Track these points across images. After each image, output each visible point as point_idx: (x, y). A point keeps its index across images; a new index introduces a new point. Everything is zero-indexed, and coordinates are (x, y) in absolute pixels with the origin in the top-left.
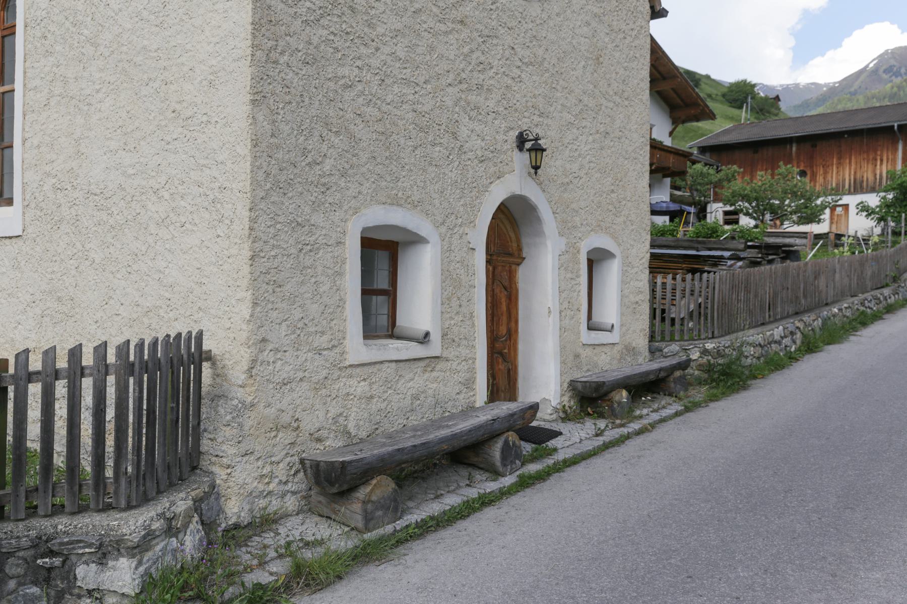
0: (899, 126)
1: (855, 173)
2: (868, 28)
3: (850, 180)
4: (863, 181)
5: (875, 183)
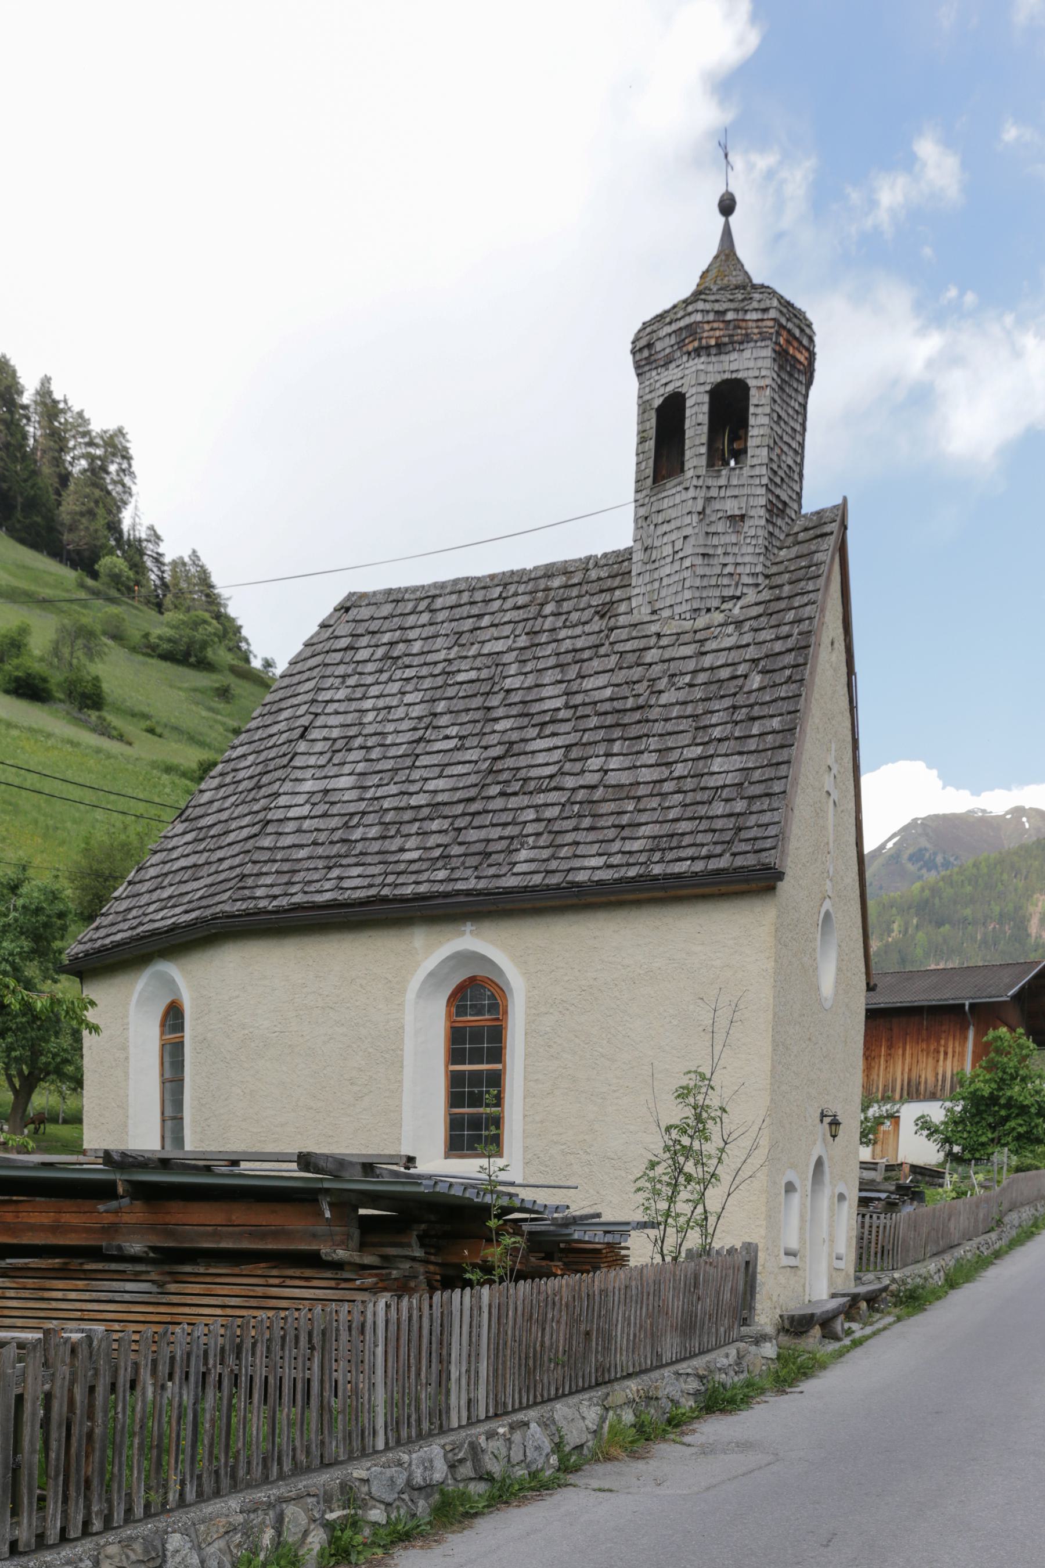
0: (971, 1005)
1: (910, 1070)
2: (884, 768)
3: (903, 1081)
4: (920, 1083)
5: (936, 1086)
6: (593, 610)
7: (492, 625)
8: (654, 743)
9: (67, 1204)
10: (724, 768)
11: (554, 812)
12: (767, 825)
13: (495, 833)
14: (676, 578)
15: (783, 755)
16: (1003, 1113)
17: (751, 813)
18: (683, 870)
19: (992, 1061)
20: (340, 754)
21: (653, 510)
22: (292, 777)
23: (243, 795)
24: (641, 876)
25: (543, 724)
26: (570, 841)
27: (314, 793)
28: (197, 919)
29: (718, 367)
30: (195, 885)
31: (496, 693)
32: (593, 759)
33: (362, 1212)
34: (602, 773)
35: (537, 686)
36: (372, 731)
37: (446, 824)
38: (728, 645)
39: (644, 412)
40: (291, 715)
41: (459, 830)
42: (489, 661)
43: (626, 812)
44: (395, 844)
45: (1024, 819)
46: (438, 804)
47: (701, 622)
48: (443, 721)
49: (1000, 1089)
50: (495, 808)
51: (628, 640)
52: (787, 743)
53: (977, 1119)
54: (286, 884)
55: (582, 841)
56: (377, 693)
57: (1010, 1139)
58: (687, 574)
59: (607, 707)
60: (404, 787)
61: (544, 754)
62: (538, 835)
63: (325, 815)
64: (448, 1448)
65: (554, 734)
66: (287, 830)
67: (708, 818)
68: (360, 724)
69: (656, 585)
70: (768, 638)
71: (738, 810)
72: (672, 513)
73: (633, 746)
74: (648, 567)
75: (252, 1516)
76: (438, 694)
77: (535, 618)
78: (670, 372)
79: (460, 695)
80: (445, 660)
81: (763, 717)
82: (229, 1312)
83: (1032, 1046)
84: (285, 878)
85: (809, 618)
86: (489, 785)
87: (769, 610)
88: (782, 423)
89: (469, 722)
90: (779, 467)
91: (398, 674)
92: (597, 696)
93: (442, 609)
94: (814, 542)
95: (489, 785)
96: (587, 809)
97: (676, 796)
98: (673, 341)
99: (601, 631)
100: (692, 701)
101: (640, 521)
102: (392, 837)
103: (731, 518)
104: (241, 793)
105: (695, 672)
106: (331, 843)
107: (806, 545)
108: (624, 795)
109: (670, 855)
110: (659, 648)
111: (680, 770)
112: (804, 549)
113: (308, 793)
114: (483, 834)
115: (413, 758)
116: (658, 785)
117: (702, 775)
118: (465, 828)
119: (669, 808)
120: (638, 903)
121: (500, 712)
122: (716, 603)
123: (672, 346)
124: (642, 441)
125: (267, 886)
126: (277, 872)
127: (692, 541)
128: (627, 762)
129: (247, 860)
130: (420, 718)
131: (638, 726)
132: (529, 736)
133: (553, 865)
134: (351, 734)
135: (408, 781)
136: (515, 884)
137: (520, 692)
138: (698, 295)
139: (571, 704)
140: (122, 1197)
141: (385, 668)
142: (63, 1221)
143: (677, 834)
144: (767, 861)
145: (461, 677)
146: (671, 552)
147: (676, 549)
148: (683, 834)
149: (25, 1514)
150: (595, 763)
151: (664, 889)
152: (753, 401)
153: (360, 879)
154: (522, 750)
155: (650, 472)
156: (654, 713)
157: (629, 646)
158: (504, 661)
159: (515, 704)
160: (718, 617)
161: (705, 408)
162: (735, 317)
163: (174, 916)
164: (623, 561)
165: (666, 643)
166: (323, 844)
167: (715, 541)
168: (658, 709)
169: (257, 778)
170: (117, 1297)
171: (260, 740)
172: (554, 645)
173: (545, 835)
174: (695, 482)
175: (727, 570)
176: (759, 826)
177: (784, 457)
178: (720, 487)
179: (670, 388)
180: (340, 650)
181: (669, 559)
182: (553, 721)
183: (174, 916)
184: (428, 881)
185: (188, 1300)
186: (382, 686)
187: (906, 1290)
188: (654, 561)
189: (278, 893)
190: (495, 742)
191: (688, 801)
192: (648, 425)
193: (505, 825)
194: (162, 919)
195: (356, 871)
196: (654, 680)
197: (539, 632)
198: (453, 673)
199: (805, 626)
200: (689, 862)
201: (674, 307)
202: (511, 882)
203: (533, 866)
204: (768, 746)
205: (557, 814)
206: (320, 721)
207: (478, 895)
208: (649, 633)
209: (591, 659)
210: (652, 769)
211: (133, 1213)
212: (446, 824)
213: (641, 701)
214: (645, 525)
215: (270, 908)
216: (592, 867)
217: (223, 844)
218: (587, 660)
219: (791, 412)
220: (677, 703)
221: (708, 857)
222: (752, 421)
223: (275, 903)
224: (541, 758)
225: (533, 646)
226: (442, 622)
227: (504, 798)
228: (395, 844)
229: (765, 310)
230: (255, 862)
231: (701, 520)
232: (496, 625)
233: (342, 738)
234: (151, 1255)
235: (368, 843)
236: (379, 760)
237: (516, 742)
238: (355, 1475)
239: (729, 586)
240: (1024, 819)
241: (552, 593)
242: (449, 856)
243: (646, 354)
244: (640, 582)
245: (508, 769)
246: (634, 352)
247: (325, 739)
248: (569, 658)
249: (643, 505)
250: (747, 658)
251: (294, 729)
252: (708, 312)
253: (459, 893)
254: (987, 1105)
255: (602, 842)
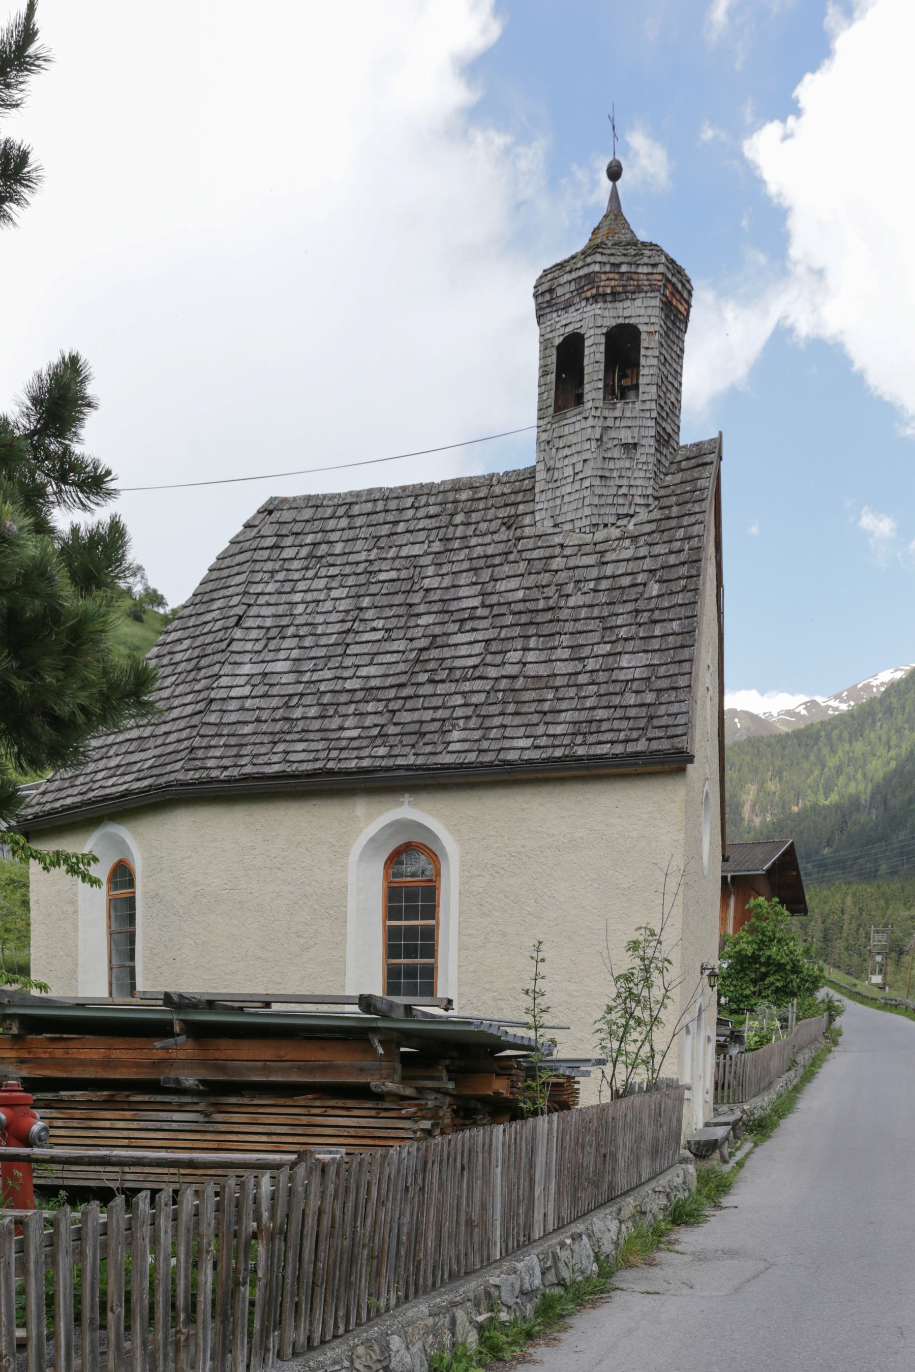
0: (732, 877)
6: (500, 521)
7: (408, 531)
8: (566, 640)
9: (117, 1042)
10: (632, 664)
11: (481, 698)
12: (676, 714)
13: (428, 715)
14: (577, 496)
15: (685, 654)
16: (763, 970)
17: (660, 704)
18: (605, 752)
19: (752, 925)
20: (275, 641)
21: (555, 435)
22: (231, 660)
23: (183, 676)
24: (567, 756)
25: (463, 621)
26: (498, 724)
27: (253, 675)
28: (150, 786)
29: (613, 313)
30: (143, 755)
31: (416, 591)
32: (512, 652)
33: (402, 1049)
34: (520, 665)
35: (454, 586)
36: (303, 622)
37: (380, 707)
38: (626, 557)
39: (546, 349)
40: (224, 605)
41: (394, 712)
42: (406, 563)
43: (547, 700)
44: (335, 723)
45: (736, 720)
46: (372, 688)
47: (600, 535)
48: (369, 614)
49: (760, 949)
50: (425, 693)
51: (534, 549)
52: (687, 644)
53: (741, 975)
54: (235, 756)
55: (509, 724)
56: (305, 588)
57: (769, 992)
58: (586, 493)
59: (521, 607)
60: (339, 673)
61: (465, 647)
62: (467, 718)
63: (265, 696)
64: (541, 1257)
65: (474, 630)
66: (230, 708)
67: (622, 707)
68: (291, 615)
69: (558, 501)
70: (663, 552)
71: (648, 701)
72: (573, 439)
73: (548, 642)
74: (550, 486)
75: (437, 1319)
76: (362, 590)
77: (447, 527)
78: (570, 315)
79: (383, 592)
80: (366, 561)
81: (665, 620)
82: (275, 1139)
83: (786, 913)
84: (234, 751)
85: (698, 536)
86: (417, 672)
87: (662, 526)
88: (667, 365)
89: (393, 616)
90: (665, 403)
91: (323, 572)
92: (511, 597)
93: (360, 515)
94: (696, 470)
95: (417, 672)
96: (510, 696)
97: (590, 687)
98: (573, 288)
99: (509, 540)
100: (598, 605)
101: (542, 444)
102: (331, 717)
103: (625, 445)
104: (180, 673)
105: (598, 579)
106: (274, 720)
107: (689, 472)
108: (543, 685)
109: (592, 739)
110: (564, 557)
111: (591, 664)
112: (688, 475)
113: (248, 675)
114: (416, 716)
115: (344, 647)
116: (572, 677)
117: (613, 670)
118: (399, 710)
119: (585, 697)
120: (562, 780)
121: (422, 609)
122: (612, 520)
123: (572, 292)
124: (544, 374)
125: (216, 758)
126: (225, 745)
127: (591, 464)
128: (543, 656)
129: (195, 734)
130: (347, 612)
131: (551, 625)
132: (450, 631)
133: (485, 745)
134: (283, 623)
135: (341, 667)
136: (452, 761)
137: (439, 591)
138: (593, 248)
139: (487, 604)
140: (179, 1035)
141: (311, 566)
142: (113, 1056)
143: (596, 721)
144: (680, 745)
145: (383, 576)
146: (572, 473)
147: (576, 471)
148: (600, 721)
149: (303, 1319)
150: (513, 656)
151: (587, 768)
152: (644, 344)
153: (305, 753)
154: (445, 643)
155: (551, 401)
156: (564, 614)
157: (536, 554)
158: (421, 563)
159: (435, 602)
160: (615, 533)
161: (602, 348)
162: (629, 270)
163: (125, 783)
164: (524, 480)
165: (569, 553)
166: (266, 721)
167: (611, 465)
168: (567, 611)
169: (195, 661)
170: (165, 1126)
171: (193, 626)
172: (467, 551)
173: (474, 719)
174: (593, 412)
175: (621, 492)
176: (669, 715)
177: (668, 395)
178: (616, 418)
179: (569, 329)
180: (267, 548)
181: (570, 480)
182: (471, 618)
183: (125, 783)
184: (370, 756)
185: (236, 1128)
186: (309, 582)
187: (755, 1120)
188: (556, 481)
189: (228, 764)
190: (420, 635)
191: (602, 692)
192: (549, 360)
193: (436, 708)
194: (113, 785)
195: (301, 746)
196: (561, 585)
197: (451, 539)
198: (375, 572)
199: (695, 543)
200: (609, 745)
201: (573, 257)
202: (448, 759)
203: (466, 746)
204: (670, 646)
205: (483, 700)
206: (254, 611)
207: (417, 770)
208: (553, 544)
209: (501, 564)
210: (566, 663)
211: (181, 1048)
212: (380, 707)
213: (551, 603)
214: (547, 448)
215: (222, 777)
216: (520, 747)
217: (167, 719)
218: (498, 565)
219: (674, 355)
220: (584, 606)
221: (626, 741)
222: (643, 361)
223: (225, 773)
224: (463, 651)
225: (447, 551)
226: (361, 527)
227: (433, 685)
228: (335, 723)
229: (654, 265)
230: (202, 736)
231: (599, 447)
232: (411, 532)
233: (275, 627)
234: (201, 1088)
235: (308, 722)
236: (312, 647)
237: (439, 636)
238: (491, 1282)
239: (623, 505)
240: (736, 720)
241: (461, 505)
242: (386, 735)
243: (547, 298)
244: (543, 498)
245: (434, 659)
246: (536, 296)
247: (259, 627)
248: (481, 563)
249: (545, 431)
250: (645, 568)
251: (228, 618)
252: (605, 263)
253: (399, 767)
254: (749, 963)
255: (527, 725)
